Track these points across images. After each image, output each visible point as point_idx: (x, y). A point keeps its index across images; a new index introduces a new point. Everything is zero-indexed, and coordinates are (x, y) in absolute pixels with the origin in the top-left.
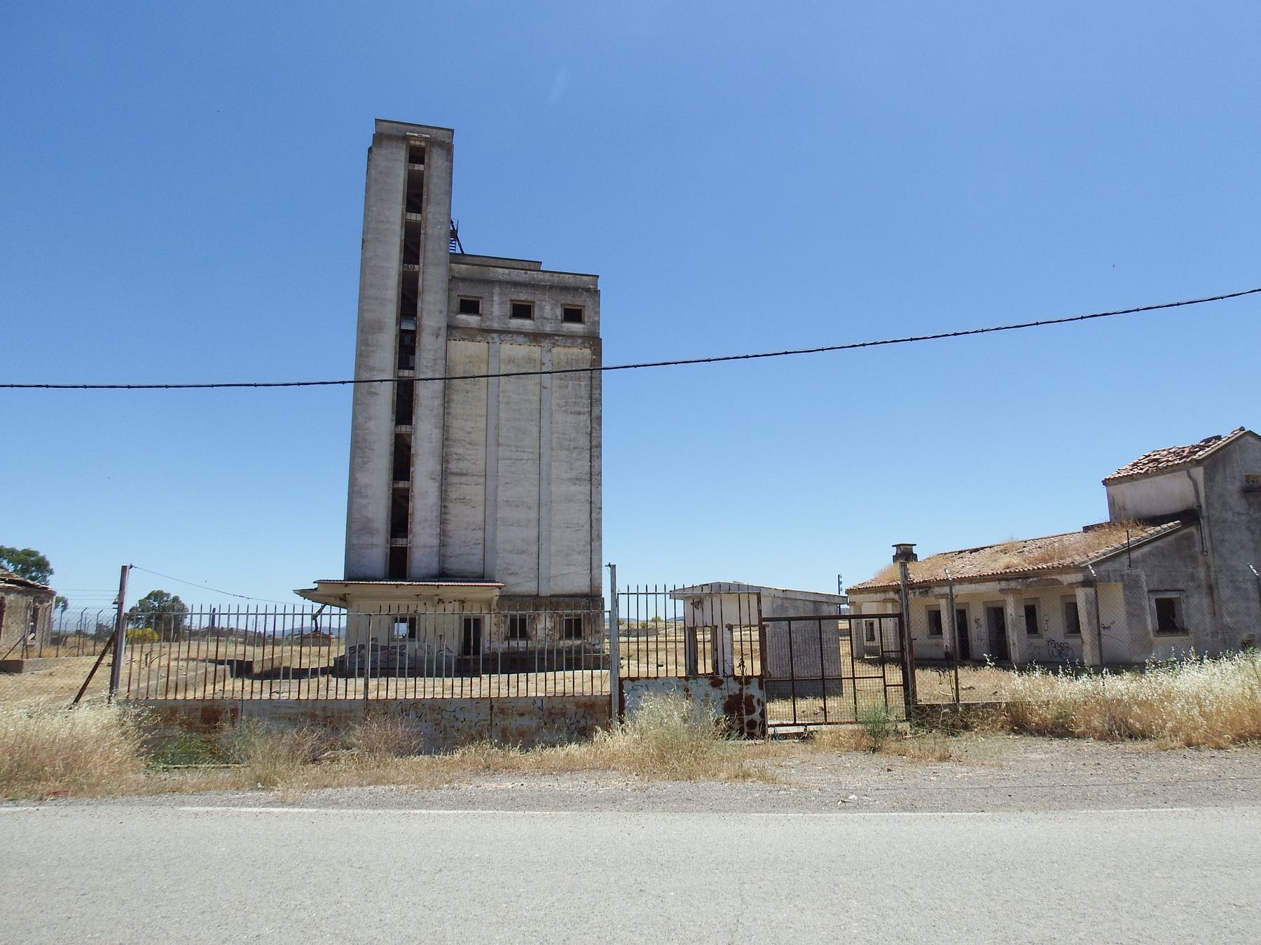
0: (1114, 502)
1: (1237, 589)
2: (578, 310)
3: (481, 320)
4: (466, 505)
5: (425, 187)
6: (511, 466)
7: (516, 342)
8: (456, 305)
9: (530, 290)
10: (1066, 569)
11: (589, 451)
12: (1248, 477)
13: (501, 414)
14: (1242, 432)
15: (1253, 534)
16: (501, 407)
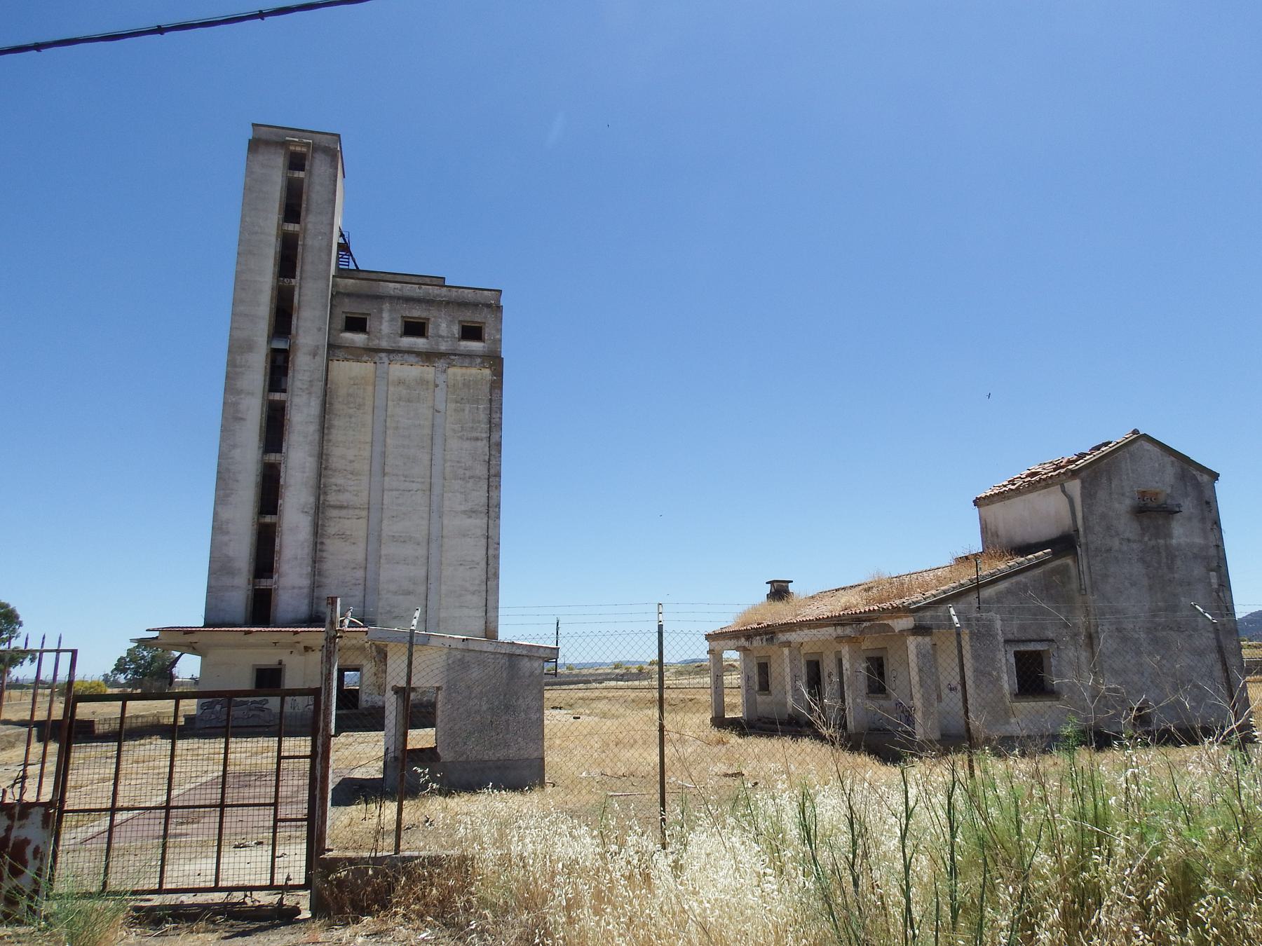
0: (986, 527)
1: (1125, 639)
2: (479, 327)
3: (368, 339)
4: (345, 541)
5: (304, 197)
6: (398, 498)
7: (406, 362)
8: (340, 322)
9: (424, 307)
10: (897, 611)
11: (487, 481)
12: (1143, 494)
13: (389, 441)
14: (1136, 436)
15: (1149, 567)
16: (388, 432)
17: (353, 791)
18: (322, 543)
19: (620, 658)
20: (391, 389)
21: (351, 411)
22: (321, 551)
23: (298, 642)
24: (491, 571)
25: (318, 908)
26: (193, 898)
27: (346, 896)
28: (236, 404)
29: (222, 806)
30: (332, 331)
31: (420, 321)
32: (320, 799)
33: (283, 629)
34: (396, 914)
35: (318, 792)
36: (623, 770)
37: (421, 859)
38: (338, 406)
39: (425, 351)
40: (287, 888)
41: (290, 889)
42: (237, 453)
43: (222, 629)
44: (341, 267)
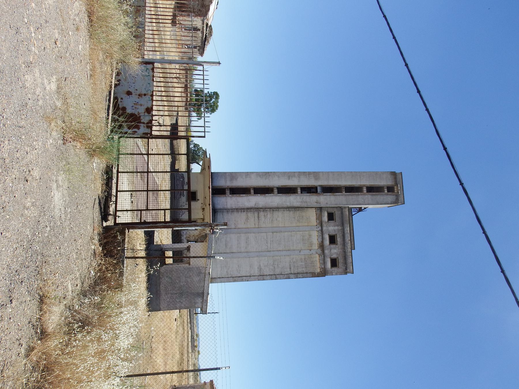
3: (326, 222)
5: (377, 193)
8: (331, 211)
11: (274, 274)
13: (286, 233)
16: (289, 233)
17: (150, 236)
18: (244, 211)
19: (200, 335)
20: (307, 232)
21: (296, 218)
22: (241, 211)
23: (206, 206)
24: (236, 279)
25: (107, 229)
26: (114, 183)
27: (110, 239)
28: (294, 176)
29: (147, 191)
30: (327, 208)
31: (336, 241)
32: (148, 226)
33: (211, 200)
34: (102, 260)
35: (151, 225)
36: (154, 346)
37: (123, 268)
38: (298, 213)
39: (324, 244)
40: (115, 216)
41: (115, 218)
42: (276, 178)
43: (210, 179)
44: (353, 209)
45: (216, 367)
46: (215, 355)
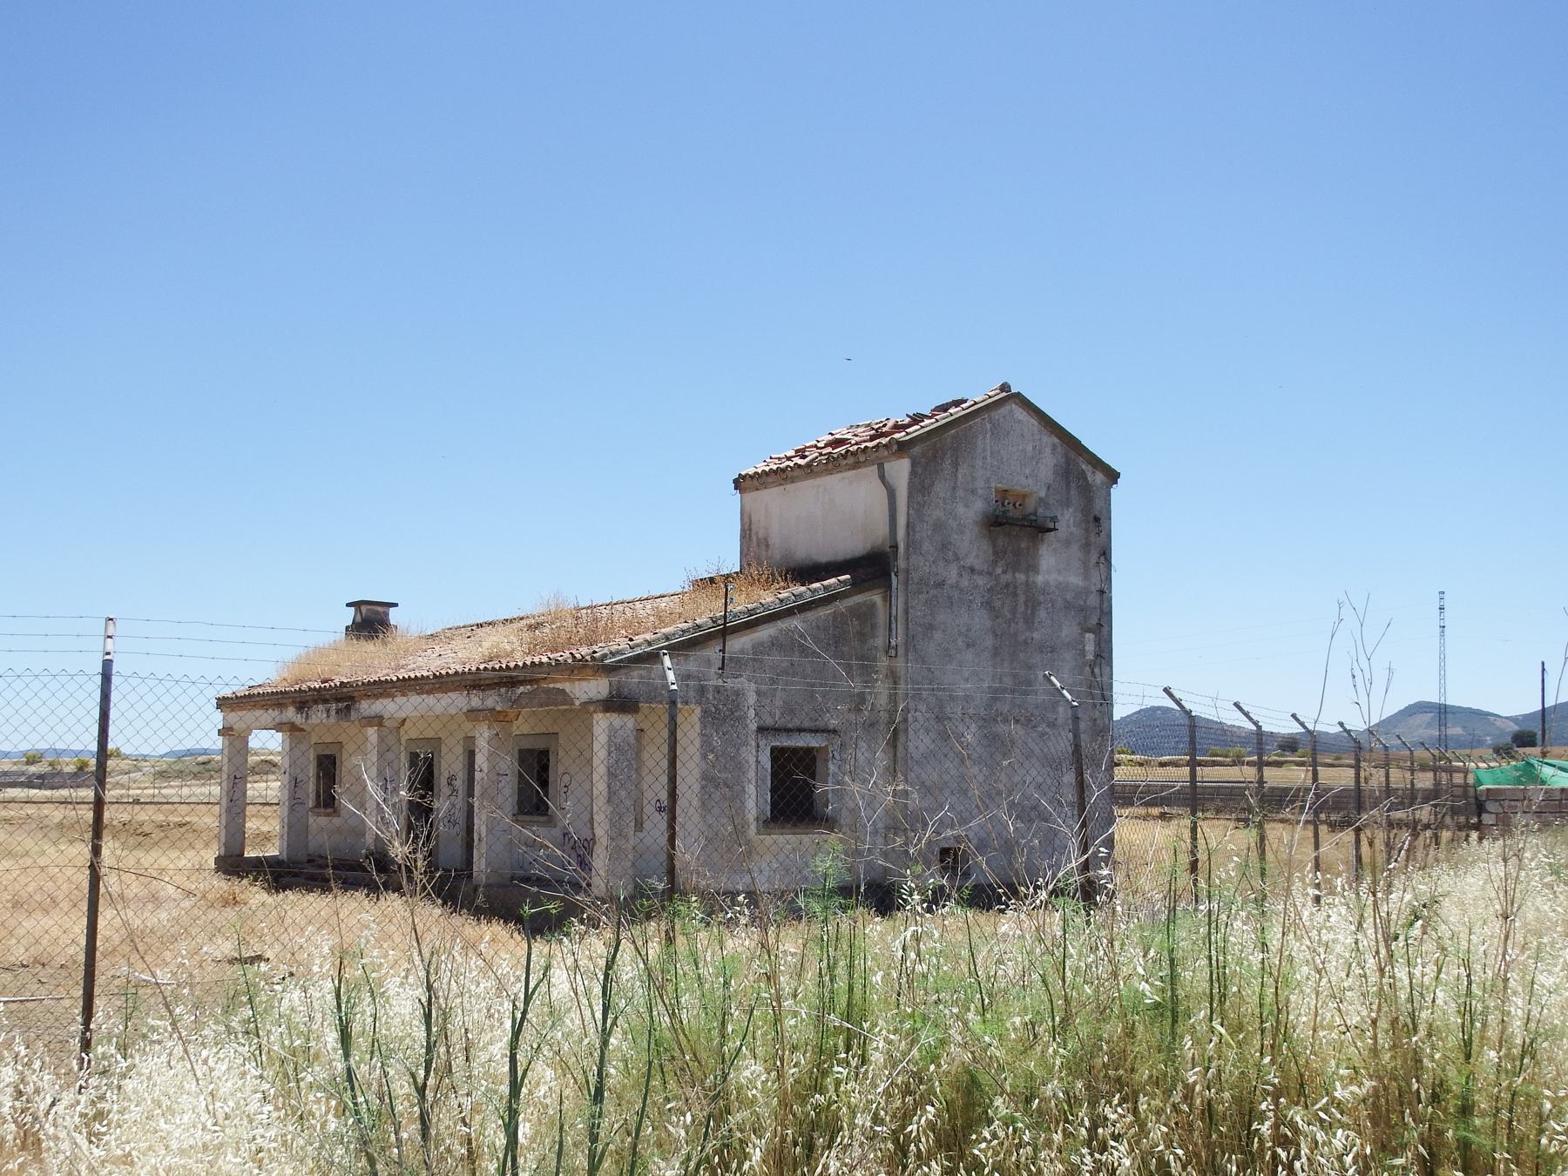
10: (579, 668)
14: (1004, 394)
15: (997, 617)
45: (99, 679)
46: (185, 686)
